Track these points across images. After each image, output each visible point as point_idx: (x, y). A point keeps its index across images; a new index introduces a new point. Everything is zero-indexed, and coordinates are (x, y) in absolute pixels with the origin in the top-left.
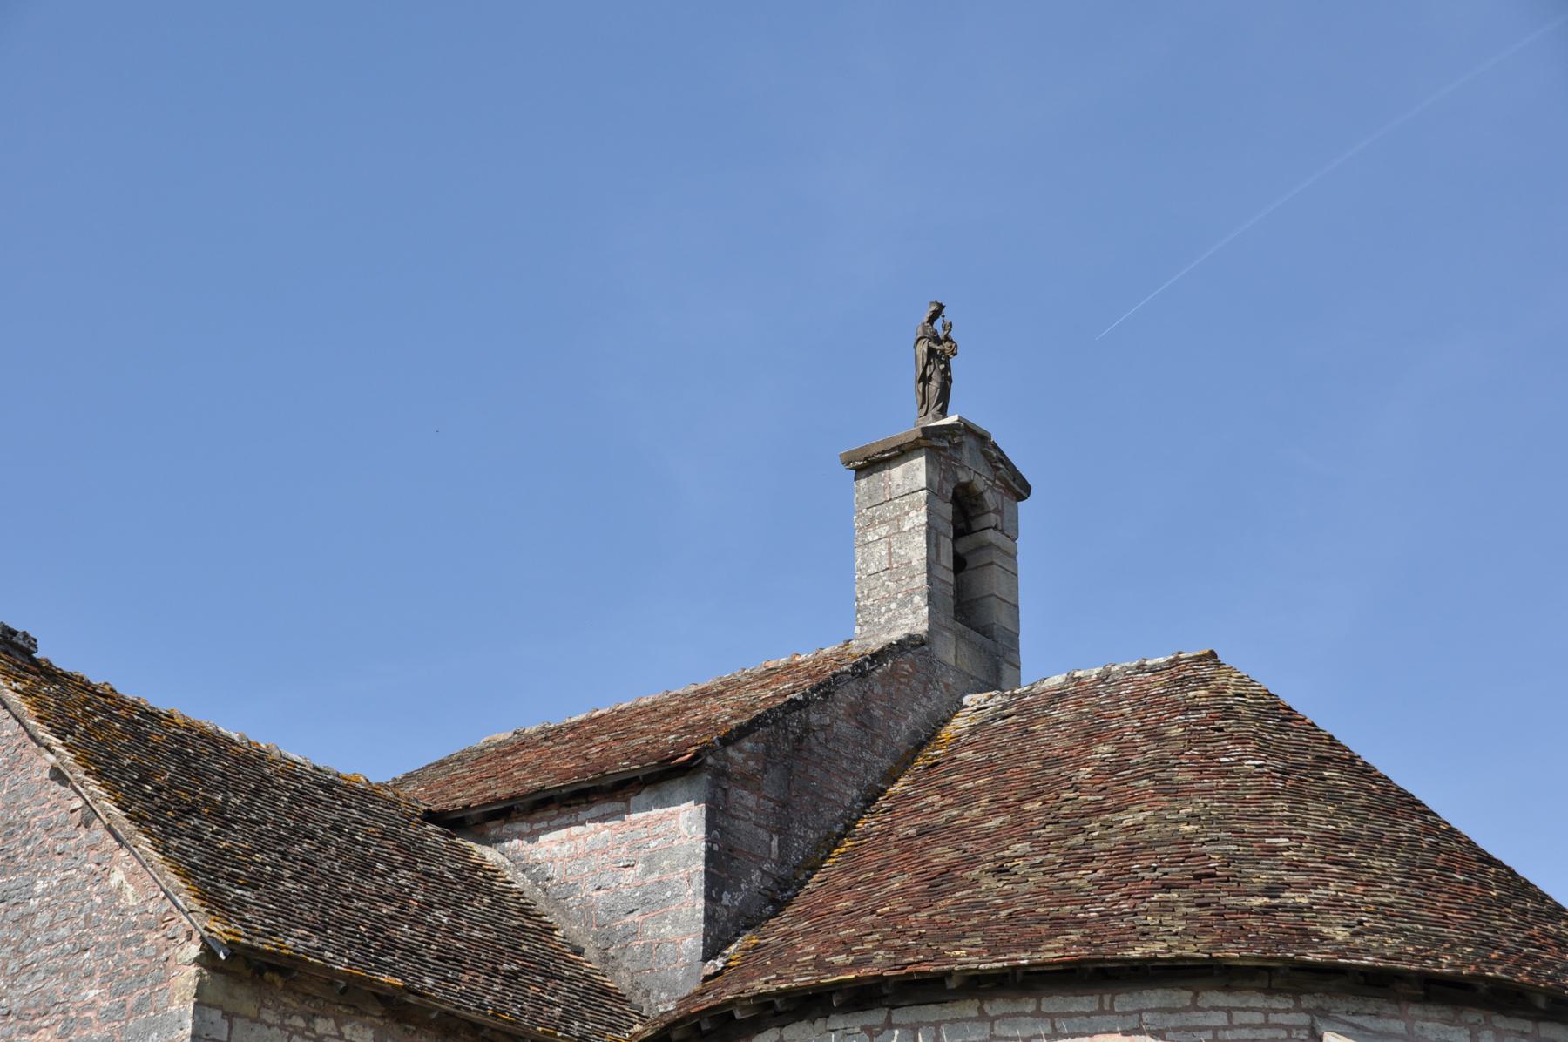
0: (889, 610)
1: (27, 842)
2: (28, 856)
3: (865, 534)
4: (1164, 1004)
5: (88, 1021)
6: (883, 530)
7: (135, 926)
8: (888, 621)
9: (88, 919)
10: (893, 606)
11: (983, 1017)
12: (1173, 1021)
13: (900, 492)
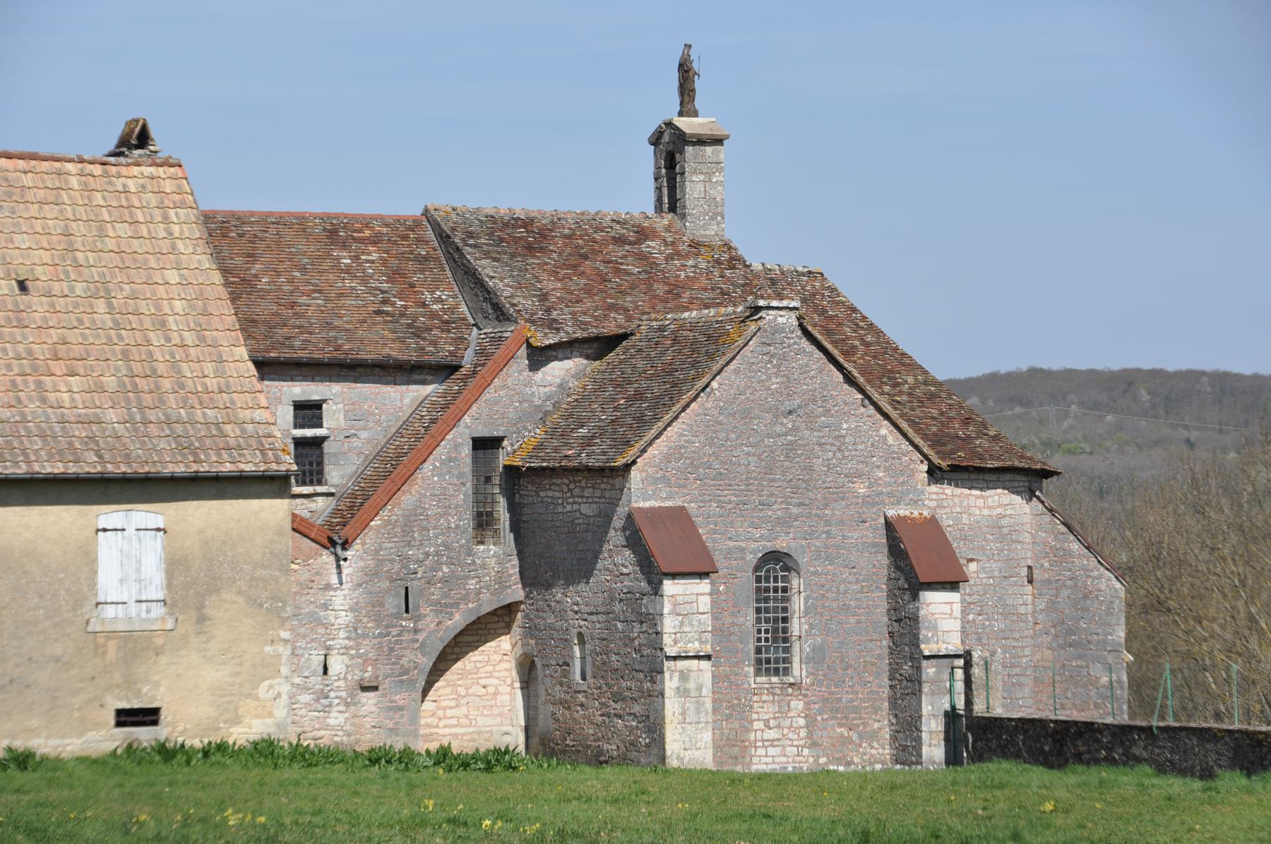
0: (704, 219)
1: (834, 406)
2: (836, 412)
3: (691, 176)
4: (1012, 479)
5: (880, 485)
6: (702, 177)
7: (896, 453)
8: (704, 224)
9: (873, 445)
10: (707, 218)
11: (970, 479)
13: (710, 160)
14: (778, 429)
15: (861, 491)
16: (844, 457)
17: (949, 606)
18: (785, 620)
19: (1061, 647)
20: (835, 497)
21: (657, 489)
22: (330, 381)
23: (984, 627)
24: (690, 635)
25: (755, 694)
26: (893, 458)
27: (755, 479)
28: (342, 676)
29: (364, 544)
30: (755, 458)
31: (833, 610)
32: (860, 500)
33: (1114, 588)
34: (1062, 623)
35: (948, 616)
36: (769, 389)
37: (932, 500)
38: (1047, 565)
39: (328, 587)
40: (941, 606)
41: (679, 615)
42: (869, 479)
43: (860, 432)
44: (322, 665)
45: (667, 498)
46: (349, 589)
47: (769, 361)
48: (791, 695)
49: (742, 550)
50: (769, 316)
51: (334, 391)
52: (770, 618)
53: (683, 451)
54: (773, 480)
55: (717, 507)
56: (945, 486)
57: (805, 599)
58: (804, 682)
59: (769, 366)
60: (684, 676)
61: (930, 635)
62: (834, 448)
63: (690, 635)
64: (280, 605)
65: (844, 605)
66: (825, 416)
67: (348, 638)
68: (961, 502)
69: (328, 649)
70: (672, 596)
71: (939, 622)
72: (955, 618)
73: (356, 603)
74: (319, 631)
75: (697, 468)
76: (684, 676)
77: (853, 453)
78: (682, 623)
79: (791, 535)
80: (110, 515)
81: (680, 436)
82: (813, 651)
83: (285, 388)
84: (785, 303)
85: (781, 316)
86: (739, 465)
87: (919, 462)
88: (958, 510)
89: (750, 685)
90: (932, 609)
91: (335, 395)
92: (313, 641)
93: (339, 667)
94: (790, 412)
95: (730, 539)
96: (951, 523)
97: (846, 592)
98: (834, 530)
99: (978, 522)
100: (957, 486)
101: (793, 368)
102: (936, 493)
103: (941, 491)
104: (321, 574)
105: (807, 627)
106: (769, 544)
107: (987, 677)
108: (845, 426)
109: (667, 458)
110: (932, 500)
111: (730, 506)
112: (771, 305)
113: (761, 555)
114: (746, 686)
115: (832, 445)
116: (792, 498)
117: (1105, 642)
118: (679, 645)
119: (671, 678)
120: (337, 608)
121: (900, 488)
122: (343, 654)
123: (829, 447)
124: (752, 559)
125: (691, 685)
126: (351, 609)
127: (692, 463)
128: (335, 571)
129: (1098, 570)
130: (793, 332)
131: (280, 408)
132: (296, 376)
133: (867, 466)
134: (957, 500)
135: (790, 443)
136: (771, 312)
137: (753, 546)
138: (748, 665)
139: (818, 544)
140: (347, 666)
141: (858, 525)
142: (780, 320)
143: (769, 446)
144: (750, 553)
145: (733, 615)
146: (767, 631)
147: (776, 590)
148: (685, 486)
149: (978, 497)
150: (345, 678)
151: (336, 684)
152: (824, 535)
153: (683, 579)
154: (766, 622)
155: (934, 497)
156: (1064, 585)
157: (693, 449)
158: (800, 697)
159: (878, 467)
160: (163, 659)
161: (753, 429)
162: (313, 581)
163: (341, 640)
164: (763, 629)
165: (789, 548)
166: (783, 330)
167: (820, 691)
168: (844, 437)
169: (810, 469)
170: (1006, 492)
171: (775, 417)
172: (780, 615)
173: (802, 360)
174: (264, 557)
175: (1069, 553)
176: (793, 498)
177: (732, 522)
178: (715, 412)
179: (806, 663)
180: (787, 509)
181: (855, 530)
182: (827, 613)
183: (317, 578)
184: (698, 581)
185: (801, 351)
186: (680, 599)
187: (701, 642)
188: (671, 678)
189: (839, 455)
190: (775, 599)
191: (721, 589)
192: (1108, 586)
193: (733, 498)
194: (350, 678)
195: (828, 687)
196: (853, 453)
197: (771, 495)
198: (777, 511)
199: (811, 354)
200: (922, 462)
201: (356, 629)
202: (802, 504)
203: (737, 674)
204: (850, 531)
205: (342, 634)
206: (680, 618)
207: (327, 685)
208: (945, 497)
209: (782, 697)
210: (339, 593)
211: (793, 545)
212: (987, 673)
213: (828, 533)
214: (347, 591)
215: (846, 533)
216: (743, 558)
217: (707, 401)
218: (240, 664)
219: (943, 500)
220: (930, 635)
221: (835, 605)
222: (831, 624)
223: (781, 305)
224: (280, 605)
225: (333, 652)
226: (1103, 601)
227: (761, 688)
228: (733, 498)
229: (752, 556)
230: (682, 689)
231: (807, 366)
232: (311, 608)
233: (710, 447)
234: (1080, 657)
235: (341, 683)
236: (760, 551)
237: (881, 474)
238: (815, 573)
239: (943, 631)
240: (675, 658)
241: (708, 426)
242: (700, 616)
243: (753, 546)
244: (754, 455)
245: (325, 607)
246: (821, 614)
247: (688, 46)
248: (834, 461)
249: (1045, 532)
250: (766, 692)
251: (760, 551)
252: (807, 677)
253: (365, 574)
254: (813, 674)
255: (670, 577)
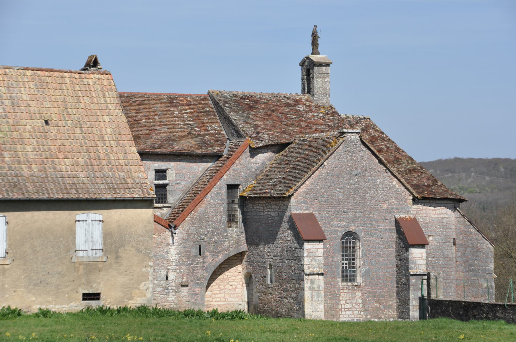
1: (374, 172)
6: (321, 79)
7: (400, 192)
8: (322, 98)
9: (390, 188)
10: (323, 96)
12: (447, 205)
13: (324, 72)
14: (351, 182)
15: (385, 207)
16: (378, 193)
17: (421, 255)
18: (354, 259)
19: (467, 271)
20: (374, 209)
21: (301, 206)
22: (170, 161)
23: (435, 263)
24: (315, 265)
25: (341, 290)
26: (398, 194)
27: (342, 202)
28: (174, 281)
29: (183, 227)
30: (342, 194)
31: (373, 255)
32: (385, 211)
33: (489, 247)
34: (468, 262)
35: (421, 258)
36: (347, 165)
37: (414, 211)
38: (461, 238)
39: (168, 244)
40: (417, 254)
41: (310, 257)
42: (388, 202)
43: (385, 183)
44: (166, 276)
45: (306, 210)
46: (177, 246)
47: (348, 154)
48: (356, 290)
49: (336, 231)
50: (348, 136)
51: (171, 165)
52: (347, 258)
53: (312, 190)
54: (349, 203)
55: (326, 213)
56: (420, 205)
57: (362, 251)
58: (361, 285)
59: (348, 156)
60: (312, 282)
61: (413, 266)
62: (374, 190)
63: (315, 265)
64: (149, 252)
65: (378, 253)
66: (370, 176)
67: (176, 265)
68: (426, 212)
69: (168, 270)
70: (308, 249)
71: (417, 261)
72: (424, 259)
73: (180, 251)
74: (165, 262)
75: (318, 197)
76: (312, 282)
77: (382, 192)
78: (312, 260)
79: (356, 225)
80: (81, 215)
81: (311, 184)
82: (365, 272)
83: (151, 164)
84: (354, 131)
85: (353, 136)
86: (335, 196)
87: (409, 196)
88: (425, 215)
89: (339, 286)
90: (414, 255)
91: (171, 167)
92: (162, 266)
93: (173, 277)
94: (356, 175)
95: (331, 226)
96: (422, 220)
97: (379, 248)
98: (374, 223)
99: (433, 220)
100: (424, 205)
101: (357, 157)
102: (416, 208)
103: (418, 207)
104: (166, 239)
105: (363, 262)
106: (347, 228)
107: (436, 283)
108: (379, 181)
109: (306, 193)
110: (414, 211)
111: (331, 213)
112: (349, 131)
113: (344, 233)
114: (338, 286)
115: (373, 188)
116: (357, 210)
117: (485, 270)
118: (310, 269)
119: (307, 283)
120: (172, 253)
121: (401, 206)
122: (174, 272)
123: (372, 189)
124: (340, 234)
125: (315, 286)
126: (178, 254)
127: (316, 195)
128: (171, 238)
129: (483, 240)
130: (357, 142)
131: (149, 172)
132: (156, 159)
133: (387, 197)
134: (424, 211)
135: (356, 187)
136: (349, 134)
137: (341, 229)
138: (339, 278)
139: (367, 228)
140: (176, 277)
141: (384, 221)
142: (352, 137)
143: (347, 189)
144: (340, 232)
145: (332, 257)
146: (346, 264)
147: (350, 247)
148: (313, 205)
149: (433, 210)
150: (175, 282)
151: (171, 284)
152: (370, 225)
153: (312, 242)
154: (346, 260)
155: (415, 210)
156: (469, 246)
157: (317, 190)
158: (360, 291)
159: (392, 197)
160: (102, 273)
161: (341, 182)
162: (162, 242)
163: (173, 266)
164: (345, 263)
165: (356, 230)
166: (353, 142)
167: (367, 288)
168: (378, 185)
169: (364, 198)
170: (445, 208)
171: (350, 177)
172: (352, 257)
173: (361, 154)
174: (142, 232)
175: (470, 233)
176: (357, 210)
177: (332, 219)
178: (326, 175)
179: (362, 277)
180: (355, 214)
181: (382, 223)
182: (371, 257)
183: (164, 241)
184: (318, 243)
185: (361, 150)
186: (311, 251)
187: (319, 268)
188: (307, 283)
189: (376, 193)
190: (350, 251)
191: (328, 247)
192: (486, 247)
193: (333, 210)
194: (177, 282)
195: (371, 287)
196: (382, 192)
197: (348, 208)
198: (351, 215)
199: (365, 152)
200: (410, 195)
201: (179, 262)
202: (361, 212)
203: (334, 281)
204: (380, 223)
205: (174, 264)
206: (311, 258)
207: (168, 284)
208: (419, 210)
209: (352, 291)
210: (173, 247)
211: (357, 229)
212: (436, 282)
213: (371, 224)
214: (176, 246)
215: (379, 224)
216: (337, 234)
217: (322, 170)
218: (133, 276)
219: (419, 211)
220: (413, 266)
221: (374, 253)
222: (373, 261)
223: (353, 131)
224: (149, 252)
225: (170, 271)
226: (484, 253)
227: (344, 287)
228: (333, 210)
229: (340, 233)
230: (311, 287)
231: (363, 156)
232: (162, 253)
233: (324, 189)
234: (475, 276)
235: (173, 284)
236: (343, 231)
237: (393, 200)
238: (366, 241)
239: (419, 265)
240: (309, 275)
241: (323, 180)
242: (319, 257)
243: (341, 229)
244: (341, 192)
245: (167, 253)
246: (369, 258)
247: (316, 26)
248: (374, 195)
249: (461, 224)
250: (346, 289)
251: (343, 231)
252: (363, 283)
253: (183, 240)
254: (365, 282)
255: (307, 242)
